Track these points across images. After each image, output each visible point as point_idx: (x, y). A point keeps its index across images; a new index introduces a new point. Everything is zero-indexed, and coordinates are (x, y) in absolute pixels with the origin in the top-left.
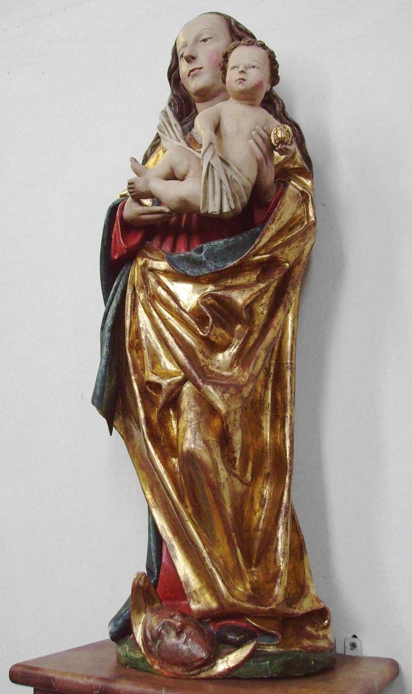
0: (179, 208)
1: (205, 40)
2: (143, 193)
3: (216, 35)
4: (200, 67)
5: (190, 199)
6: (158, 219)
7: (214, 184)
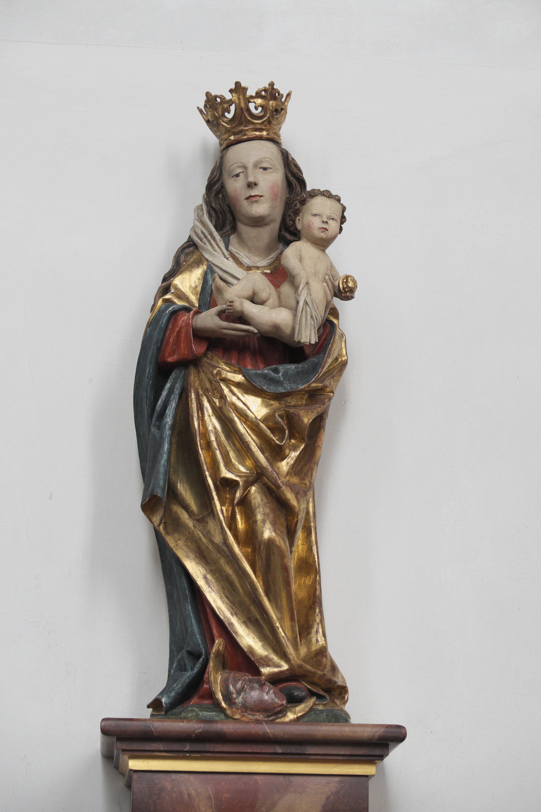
0: (270, 332)
1: (265, 169)
2: (238, 311)
3: (275, 166)
4: (261, 195)
5: (282, 326)
6: (239, 337)
7: (306, 319)
